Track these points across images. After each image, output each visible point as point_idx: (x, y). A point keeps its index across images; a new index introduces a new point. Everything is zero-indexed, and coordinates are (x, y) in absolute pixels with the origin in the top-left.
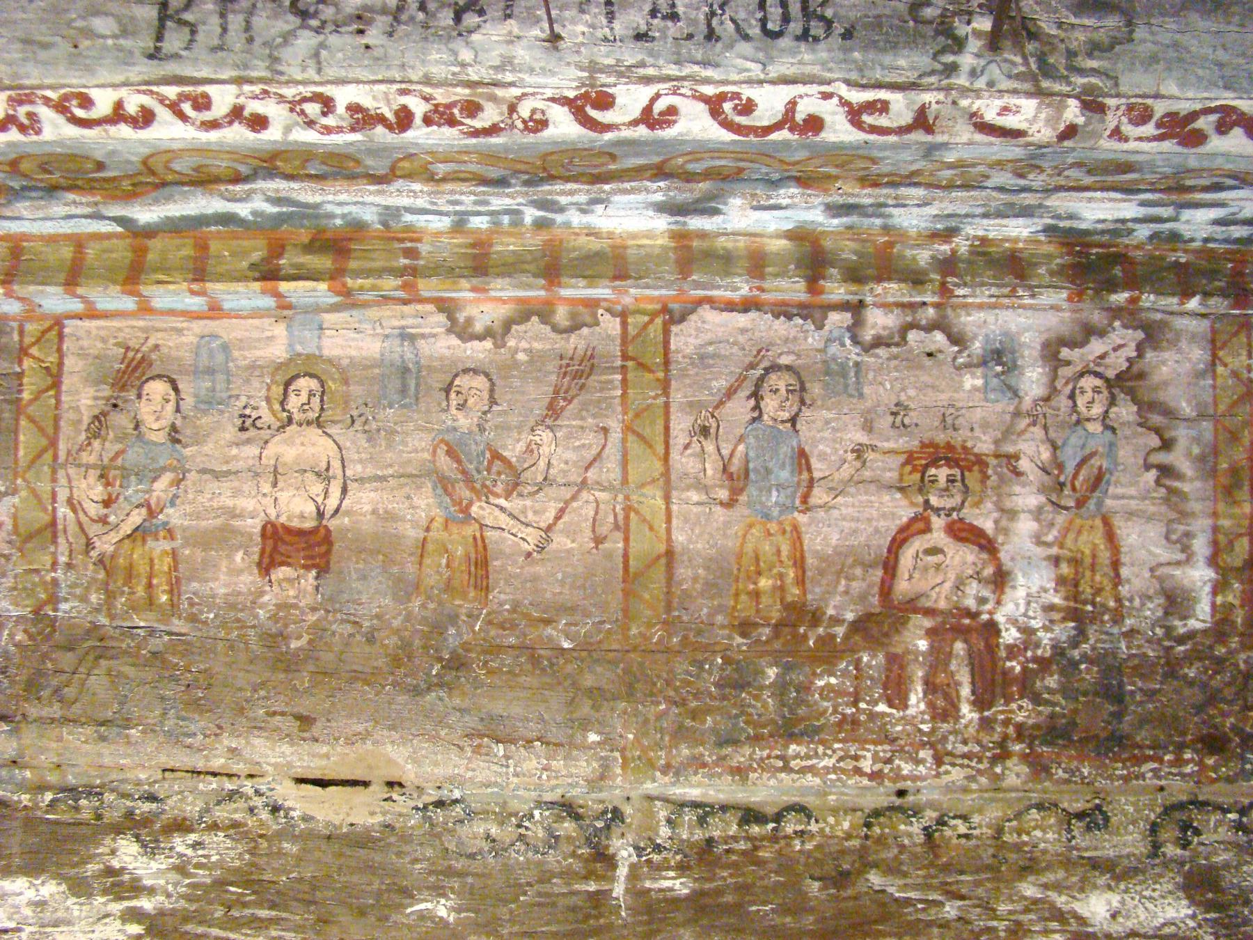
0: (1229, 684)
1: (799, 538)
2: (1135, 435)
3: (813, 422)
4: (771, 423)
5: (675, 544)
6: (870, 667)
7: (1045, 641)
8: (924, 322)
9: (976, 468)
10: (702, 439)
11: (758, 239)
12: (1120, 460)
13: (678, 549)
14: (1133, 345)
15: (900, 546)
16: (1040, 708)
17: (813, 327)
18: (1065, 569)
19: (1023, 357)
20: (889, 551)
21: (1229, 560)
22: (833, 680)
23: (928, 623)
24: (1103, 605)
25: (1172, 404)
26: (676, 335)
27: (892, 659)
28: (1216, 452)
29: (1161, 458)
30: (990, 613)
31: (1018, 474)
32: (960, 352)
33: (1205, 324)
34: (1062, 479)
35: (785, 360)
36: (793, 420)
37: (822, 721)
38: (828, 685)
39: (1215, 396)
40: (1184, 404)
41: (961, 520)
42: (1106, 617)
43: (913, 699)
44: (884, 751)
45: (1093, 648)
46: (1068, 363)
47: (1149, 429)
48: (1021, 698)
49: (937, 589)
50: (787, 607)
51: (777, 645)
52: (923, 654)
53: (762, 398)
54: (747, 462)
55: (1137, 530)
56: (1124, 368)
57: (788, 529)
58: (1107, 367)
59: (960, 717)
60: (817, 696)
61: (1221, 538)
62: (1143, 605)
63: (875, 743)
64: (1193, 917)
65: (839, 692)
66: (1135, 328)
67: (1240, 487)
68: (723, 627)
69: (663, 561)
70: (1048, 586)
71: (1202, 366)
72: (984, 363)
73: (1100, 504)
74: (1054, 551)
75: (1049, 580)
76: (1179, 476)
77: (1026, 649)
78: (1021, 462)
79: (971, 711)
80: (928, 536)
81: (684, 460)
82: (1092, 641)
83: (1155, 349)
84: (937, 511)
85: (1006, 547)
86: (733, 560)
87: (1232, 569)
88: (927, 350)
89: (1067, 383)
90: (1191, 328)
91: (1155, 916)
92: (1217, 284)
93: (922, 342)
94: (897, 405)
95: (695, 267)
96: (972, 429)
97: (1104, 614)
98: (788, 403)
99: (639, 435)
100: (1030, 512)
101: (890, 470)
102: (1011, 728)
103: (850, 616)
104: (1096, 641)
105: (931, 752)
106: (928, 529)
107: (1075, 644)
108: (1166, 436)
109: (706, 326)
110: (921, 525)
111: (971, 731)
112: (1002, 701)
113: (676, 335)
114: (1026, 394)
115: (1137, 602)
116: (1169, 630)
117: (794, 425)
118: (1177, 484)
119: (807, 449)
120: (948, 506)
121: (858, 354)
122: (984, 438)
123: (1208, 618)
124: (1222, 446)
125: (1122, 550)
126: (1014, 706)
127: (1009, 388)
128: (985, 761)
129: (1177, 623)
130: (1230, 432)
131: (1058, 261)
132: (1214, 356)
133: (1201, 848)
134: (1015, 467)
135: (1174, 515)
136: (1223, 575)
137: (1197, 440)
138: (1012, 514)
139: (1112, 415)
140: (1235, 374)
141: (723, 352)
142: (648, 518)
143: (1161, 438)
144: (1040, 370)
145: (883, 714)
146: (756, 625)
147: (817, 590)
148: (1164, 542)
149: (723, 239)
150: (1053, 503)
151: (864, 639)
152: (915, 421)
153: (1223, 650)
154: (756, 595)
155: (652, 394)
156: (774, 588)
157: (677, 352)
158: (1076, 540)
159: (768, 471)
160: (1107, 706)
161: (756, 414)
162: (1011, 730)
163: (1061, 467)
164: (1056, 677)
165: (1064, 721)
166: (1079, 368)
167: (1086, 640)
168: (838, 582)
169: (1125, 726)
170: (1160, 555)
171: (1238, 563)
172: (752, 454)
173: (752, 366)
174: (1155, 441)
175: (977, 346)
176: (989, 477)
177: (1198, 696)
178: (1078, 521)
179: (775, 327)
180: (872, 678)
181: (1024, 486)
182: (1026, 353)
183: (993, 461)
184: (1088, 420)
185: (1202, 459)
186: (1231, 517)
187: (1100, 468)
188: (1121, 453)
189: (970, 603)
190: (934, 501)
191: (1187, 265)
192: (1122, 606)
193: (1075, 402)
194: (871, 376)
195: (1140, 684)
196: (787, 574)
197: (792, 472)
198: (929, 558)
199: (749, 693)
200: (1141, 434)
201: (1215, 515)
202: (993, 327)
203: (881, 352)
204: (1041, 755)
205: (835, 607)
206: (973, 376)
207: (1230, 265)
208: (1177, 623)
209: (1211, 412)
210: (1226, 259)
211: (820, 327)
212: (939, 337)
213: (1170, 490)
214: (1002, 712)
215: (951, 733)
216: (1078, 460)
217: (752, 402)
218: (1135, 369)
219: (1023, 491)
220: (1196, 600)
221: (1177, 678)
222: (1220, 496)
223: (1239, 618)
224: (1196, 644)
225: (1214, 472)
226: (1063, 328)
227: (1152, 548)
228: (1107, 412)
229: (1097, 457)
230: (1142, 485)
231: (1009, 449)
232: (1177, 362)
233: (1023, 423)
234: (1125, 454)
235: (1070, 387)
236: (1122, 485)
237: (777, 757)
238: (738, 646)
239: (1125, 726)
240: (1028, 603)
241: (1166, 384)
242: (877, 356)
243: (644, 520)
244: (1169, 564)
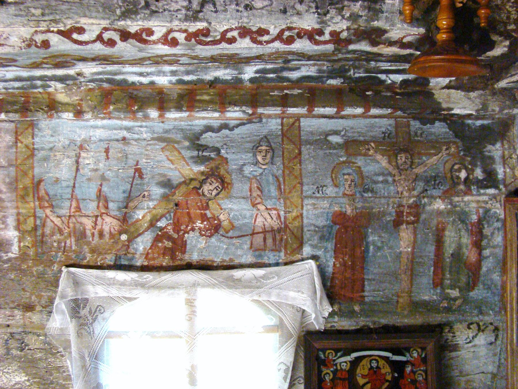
21: (25, 227)
28: (17, 180)
33: (13, 125)
39: (16, 156)
61: (21, 218)
64: (28, 380)
67: (28, 196)
71: (11, 143)
80: (39, 208)
87: (26, 231)
90: (6, 127)
91: (11, 381)
123: (17, 253)
124: (19, 178)
132: (17, 138)
133: (29, 351)
137: (8, 176)
140: (27, 147)
171: (29, 228)
185: (10, 184)
186: (25, 208)
201: (17, 207)
207: (23, 99)
209: (14, 163)
210: (21, 96)
220: (12, 245)
222: (19, 200)
224: (12, 264)
225: (16, 188)
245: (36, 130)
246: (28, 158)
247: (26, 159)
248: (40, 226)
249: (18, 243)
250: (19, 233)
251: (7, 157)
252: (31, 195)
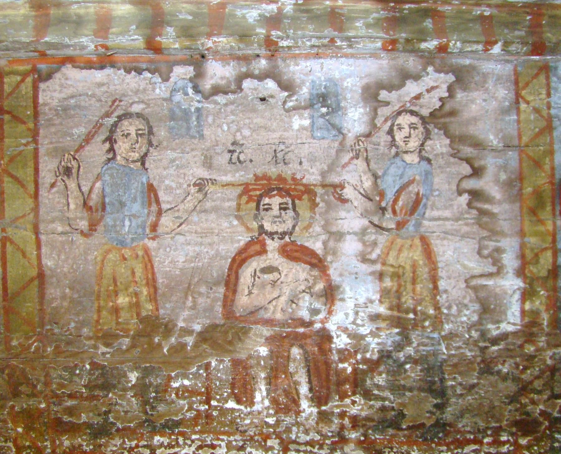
0: (537, 377)
1: (150, 261)
2: (448, 164)
3: (161, 160)
4: (123, 163)
5: (45, 269)
6: (219, 371)
7: (373, 346)
8: (257, 72)
9: (305, 197)
10: (65, 178)
11: (106, 5)
12: (435, 187)
13: (48, 273)
14: (444, 87)
15: (240, 265)
16: (372, 403)
17: (160, 80)
18: (388, 283)
19: (345, 99)
20: (230, 269)
21: (535, 270)
22: (186, 382)
23: (267, 332)
24: (423, 313)
25: (482, 137)
26: (44, 91)
27: (236, 363)
28: (521, 178)
29: (471, 184)
30: (322, 322)
31: (344, 201)
32: (289, 96)
34: (383, 204)
35: (136, 108)
36: (143, 160)
37: (180, 417)
38: (183, 386)
39: (519, 129)
40: (491, 137)
41: (293, 243)
42: (427, 324)
43: (258, 397)
44: (236, 440)
45: (417, 351)
46: (387, 104)
47: (461, 159)
48: (354, 394)
49: (274, 303)
50: (142, 320)
51: (136, 352)
52: (264, 358)
53: (116, 142)
54: (104, 197)
55: (452, 247)
56: (437, 107)
57: (140, 253)
58: (421, 107)
59: (300, 412)
60: (173, 395)
61: (529, 255)
62: (459, 311)
63: (229, 434)
65: (192, 392)
66: (447, 73)
68: (90, 338)
69: (36, 282)
70: (374, 298)
71: (507, 104)
72: (310, 106)
73: (418, 225)
74: (378, 267)
75: (374, 292)
76: (489, 199)
77: (356, 352)
78: (345, 191)
79: (309, 407)
80: (264, 257)
81: (51, 197)
82: (415, 345)
83: (464, 90)
84: (271, 235)
85: (335, 265)
86: (94, 280)
87: (538, 278)
88: (261, 96)
89: (386, 120)
90: (496, 72)
92: (517, 33)
93: (255, 89)
94: (233, 144)
95: (49, 29)
96: (301, 163)
97: (425, 320)
98: (137, 146)
99: (12, 176)
100: (355, 234)
101: (229, 200)
102: (347, 419)
103: (198, 328)
104: (418, 345)
105: (277, 441)
106: (263, 251)
107: (399, 347)
108: (476, 165)
109: (69, 82)
110: (257, 247)
111: (312, 422)
112: (337, 397)
113: (44, 91)
114: (349, 131)
115: (454, 310)
116: (483, 334)
117: (143, 164)
118: (486, 206)
119: (155, 184)
120: (280, 230)
121: (199, 102)
122: (311, 171)
123: (518, 321)
125: (440, 265)
126: (348, 401)
127: (334, 126)
128: (325, 447)
129: (490, 326)
130: (534, 161)
131: (375, 15)
132: (518, 96)
134: (341, 195)
135: (485, 233)
136: (531, 284)
137: (504, 167)
138: (339, 236)
139: (427, 148)
141: (83, 104)
142: (22, 246)
143: (472, 167)
144: (362, 110)
145: (233, 410)
146: (117, 337)
147: (168, 306)
148: (478, 256)
149: (75, 6)
150: (375, 226)
151: (212, 347)
152: (249, 156)
153: (532, 349)
154: (116, 310)
155: (24, 141)
156: (131, 306)
157: (45, 104)
158: (398, 257)
159: (122, 205)
160: (431, 399)
161: (111, 156)
162: (347, 421)
163: (382, 194)
164: (384, 375)
165: (393, 413)
166: (396, 108)
167: (409, 343)
168: (186, 298)
169: (448, 414)
170: (474, 268)
171: (544, 273)
172: (108, 190)
173: (108, 115)
174: (466, 169)
175: (305, 92)
176: (317, 205)
177: (511, 387)
178: (399, 241)
179: (127, 81)
180: (220, 380)
181: (349, 211)
182: (349, 96)
183: (320, 191)
184: (406, 152)
187: (418, 194)
188: (436, 180)
189: (304, 314)
190: (268, 227)
191: (490, 17)
192: (441, 313)
193: (393, 137)
194: (210, 119)
195: (459, 379)
196: (141, 292)
197: (143, 203)
198: (266, 276)
199: (114, 394)
200: (454, 164)
202: (319, 75)
203: (220, 99)
204: (375, 441)
205: (184, 320)
206: (301, 117)
207: (528, 18)
208: (490, 326)
209: (516, 142)
211: (166, 79)
212: (271, 85)
213: (482, 213)
214: (337, 407)
215: (293, 425)
216: (397, 187)
217: (107, 145)
218: (447, 108)
219: (348, 215)
221: (492, 374)
223: (545, 319)
225: (520, 194)
226: (382, 74)
227: (466, 262)
228: (422, 145)
229: (415, 185)
230: (455, 207)
231: (334, 179)
232: (485, 100)
233: (346, 157)
234: (438, 180)
235: (389, 124)
236: (438, 209)
237: (144, 446)
238: (104, 354)
239: (448, 414)
240: (357, 313)
241: (475, 120)
242: (216, 103)
243: (18, 248)
244: (482, 276)
245: (554, 79)
246: (541, 132)
247: (538, 135)
248: (47, 227)
249: (519, 302)
250: (525, 282)
251: (501, 130)
252: (549, 208)
